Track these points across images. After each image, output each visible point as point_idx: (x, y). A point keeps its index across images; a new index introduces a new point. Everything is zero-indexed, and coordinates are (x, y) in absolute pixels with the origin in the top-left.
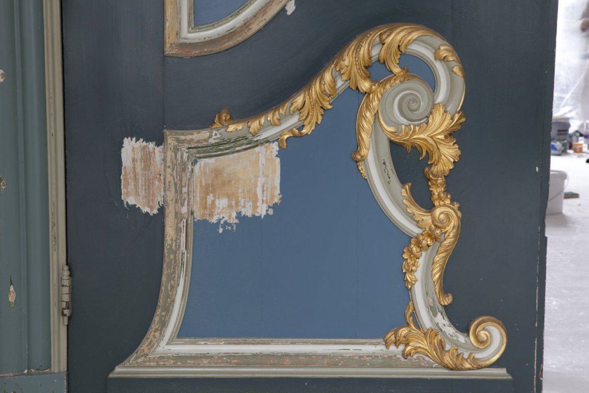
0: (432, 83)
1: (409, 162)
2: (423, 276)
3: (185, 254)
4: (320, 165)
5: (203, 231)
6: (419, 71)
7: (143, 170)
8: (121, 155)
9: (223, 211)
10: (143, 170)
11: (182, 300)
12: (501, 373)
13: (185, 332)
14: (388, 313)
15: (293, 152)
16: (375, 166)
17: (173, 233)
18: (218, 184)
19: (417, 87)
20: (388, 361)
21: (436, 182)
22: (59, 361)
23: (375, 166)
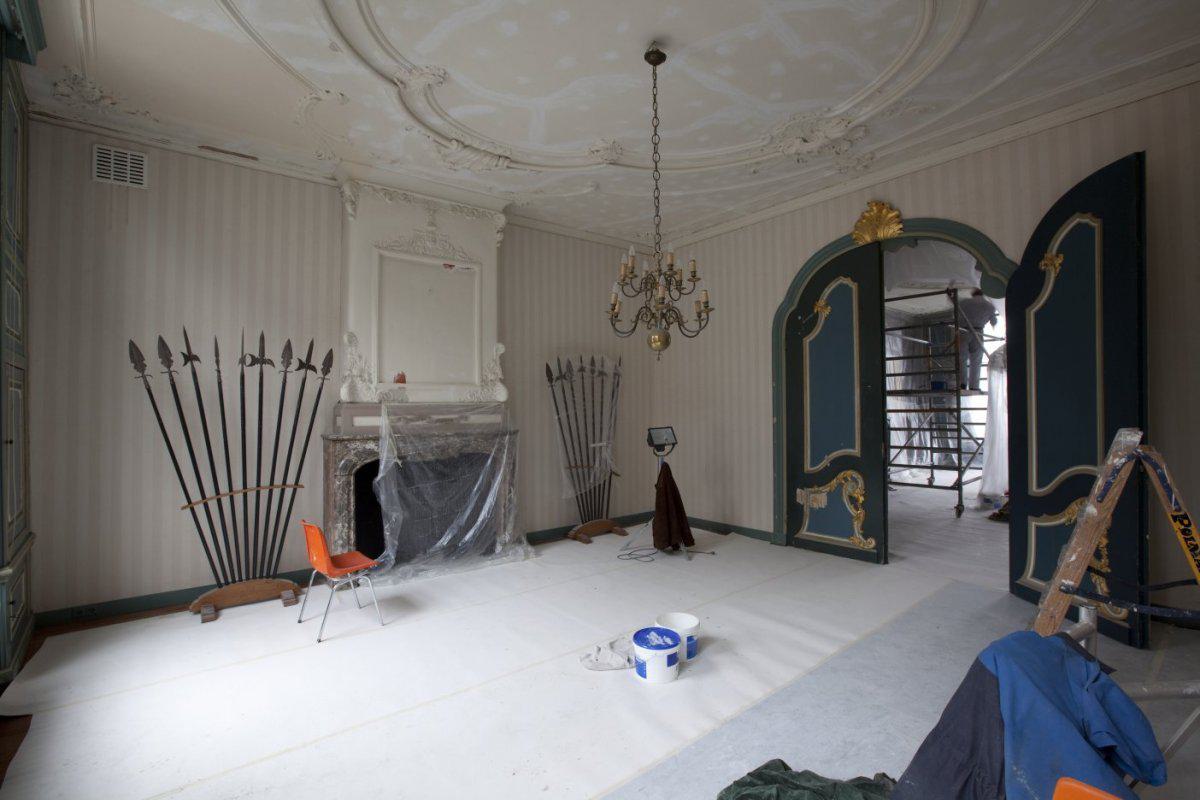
0: (857, 482)
1: (853, 500)
2: (857, 526)
3: (808, 513)
4: (834, 497)
5: (812, 509)
6: (855, 480)
7: (801, 495)
8: (672, 478)
9: (815, 506)
10: (801, 495)
11: (456, 122)
12: (875, 551)
13: (808, 530)
14: (850, 534)
15: (829, 494)
16: (845, 500)
17: (807, 511)
18: (815, 500)
19: (854, 483)
20: (849, 544)
21: (406, 418)
22: (785, 532)
23: (845, 500)
